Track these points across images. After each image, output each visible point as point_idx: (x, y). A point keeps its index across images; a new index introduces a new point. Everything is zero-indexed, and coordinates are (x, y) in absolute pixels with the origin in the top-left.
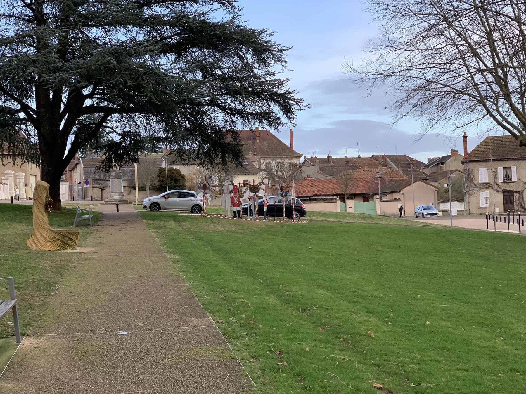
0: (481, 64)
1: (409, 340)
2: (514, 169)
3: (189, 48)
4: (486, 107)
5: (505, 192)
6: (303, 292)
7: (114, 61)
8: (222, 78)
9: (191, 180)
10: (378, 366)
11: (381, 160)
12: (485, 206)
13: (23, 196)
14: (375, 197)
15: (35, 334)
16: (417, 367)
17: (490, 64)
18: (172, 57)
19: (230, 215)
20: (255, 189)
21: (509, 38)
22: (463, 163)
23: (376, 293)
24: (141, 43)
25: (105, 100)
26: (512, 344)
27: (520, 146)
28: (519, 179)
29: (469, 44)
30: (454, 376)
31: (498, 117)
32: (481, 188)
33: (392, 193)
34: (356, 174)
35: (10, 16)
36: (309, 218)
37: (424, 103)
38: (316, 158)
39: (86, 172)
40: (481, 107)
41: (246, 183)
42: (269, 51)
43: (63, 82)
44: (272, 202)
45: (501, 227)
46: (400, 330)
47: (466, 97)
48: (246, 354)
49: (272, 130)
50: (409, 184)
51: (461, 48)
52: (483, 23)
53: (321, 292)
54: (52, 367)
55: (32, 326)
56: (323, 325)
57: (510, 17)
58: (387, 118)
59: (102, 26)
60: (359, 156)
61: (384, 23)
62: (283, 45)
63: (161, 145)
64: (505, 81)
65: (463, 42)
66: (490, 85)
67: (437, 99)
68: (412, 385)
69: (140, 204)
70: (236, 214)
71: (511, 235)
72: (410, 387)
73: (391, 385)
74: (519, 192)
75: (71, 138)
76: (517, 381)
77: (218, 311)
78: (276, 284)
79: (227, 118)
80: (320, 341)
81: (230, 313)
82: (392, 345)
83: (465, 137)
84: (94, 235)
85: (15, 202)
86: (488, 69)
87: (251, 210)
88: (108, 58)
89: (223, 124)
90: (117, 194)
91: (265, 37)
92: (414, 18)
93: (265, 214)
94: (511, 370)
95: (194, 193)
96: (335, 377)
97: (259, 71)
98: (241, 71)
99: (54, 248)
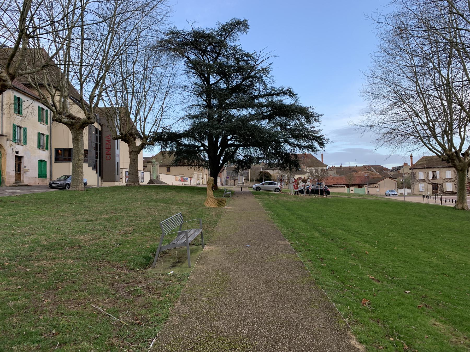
0: (420, 120)
1: (386, 256)
2: (438, 172)
3: (275, 117)
4: (423, 142)
5: (432, 184)
6: (331, 231)
7: (241, 124)
8: (290, 130)
9: (274, 177)
10: (371, 268)
11: (368, 168)
12: (422, 191)
13: (201, 183)
14: (364, 186)
15: (210, 244)
16: (391, 270)
17: (425, 120)
18: (267, 121)
19: (293, 193)
20: (305, 181)
21: (436, 108)
22: (410, 169)
23: (368, 233)
24: (253, 115)
25: (237, 141)
26: (441, 261)
27: (442, 161)
28: (441, 177)
29: (414, 112)
30: (411, 275)
31: (430, 147)
32: (420, 182)
33: (373, 184)
34: (355, 174)
35: (197, 105)
36: (332, 195)
37: (390, 140)
38: (334, 167)
39: (228, 173)
40: (421, 142)
41: (300, 179)
42: (313, 116)
43: (220, 134)
44: (313, 187)
45: (431, 202)
46: (382, 251)
47: (413, 137)
48: (306, 259)
49: (313, 154)
50: (383, 179)
51: (409, 113)
52: (422, 100)
53: (340, 231)
54: (218, 260)
55: (208, 241)
56: (342, 247)
57: (436, 97)
58: (371, 147)
59: (236, 108)
60: (356, 166)
61: (370, 102)
62: (319, 114)
63: (261, 161)
64: (434, 129)
65: (411, 110)
66: (425, 131)
67: (397, 138)
68: (389, 278)
69: (251, 187)
70: (296, 193)
71: (437, 206)
72: (389, 279)
73: (379, 278)
74: (440, 184)
75: (222, 158)
76: (446, 280)
77: (291, 238)
78: (318, 227)
79: (292, 148)
80: (341, 255)
81: (297, 239)
82: (378, 258)
83: (411, 156)
84: (232, 201)
85: (198, 186)
86: (424, 123)
87: (303, 191)
88: (239, 122)
89: (290, 151)
90: (241, 183)
91: (310, 110)
92: (385, 99)
93: (310, 193)
94: (442, 274)
95: (276, 183)
96: (350, 272)
97: (307, 126)
98: (299, 126)
99: (215, 206)
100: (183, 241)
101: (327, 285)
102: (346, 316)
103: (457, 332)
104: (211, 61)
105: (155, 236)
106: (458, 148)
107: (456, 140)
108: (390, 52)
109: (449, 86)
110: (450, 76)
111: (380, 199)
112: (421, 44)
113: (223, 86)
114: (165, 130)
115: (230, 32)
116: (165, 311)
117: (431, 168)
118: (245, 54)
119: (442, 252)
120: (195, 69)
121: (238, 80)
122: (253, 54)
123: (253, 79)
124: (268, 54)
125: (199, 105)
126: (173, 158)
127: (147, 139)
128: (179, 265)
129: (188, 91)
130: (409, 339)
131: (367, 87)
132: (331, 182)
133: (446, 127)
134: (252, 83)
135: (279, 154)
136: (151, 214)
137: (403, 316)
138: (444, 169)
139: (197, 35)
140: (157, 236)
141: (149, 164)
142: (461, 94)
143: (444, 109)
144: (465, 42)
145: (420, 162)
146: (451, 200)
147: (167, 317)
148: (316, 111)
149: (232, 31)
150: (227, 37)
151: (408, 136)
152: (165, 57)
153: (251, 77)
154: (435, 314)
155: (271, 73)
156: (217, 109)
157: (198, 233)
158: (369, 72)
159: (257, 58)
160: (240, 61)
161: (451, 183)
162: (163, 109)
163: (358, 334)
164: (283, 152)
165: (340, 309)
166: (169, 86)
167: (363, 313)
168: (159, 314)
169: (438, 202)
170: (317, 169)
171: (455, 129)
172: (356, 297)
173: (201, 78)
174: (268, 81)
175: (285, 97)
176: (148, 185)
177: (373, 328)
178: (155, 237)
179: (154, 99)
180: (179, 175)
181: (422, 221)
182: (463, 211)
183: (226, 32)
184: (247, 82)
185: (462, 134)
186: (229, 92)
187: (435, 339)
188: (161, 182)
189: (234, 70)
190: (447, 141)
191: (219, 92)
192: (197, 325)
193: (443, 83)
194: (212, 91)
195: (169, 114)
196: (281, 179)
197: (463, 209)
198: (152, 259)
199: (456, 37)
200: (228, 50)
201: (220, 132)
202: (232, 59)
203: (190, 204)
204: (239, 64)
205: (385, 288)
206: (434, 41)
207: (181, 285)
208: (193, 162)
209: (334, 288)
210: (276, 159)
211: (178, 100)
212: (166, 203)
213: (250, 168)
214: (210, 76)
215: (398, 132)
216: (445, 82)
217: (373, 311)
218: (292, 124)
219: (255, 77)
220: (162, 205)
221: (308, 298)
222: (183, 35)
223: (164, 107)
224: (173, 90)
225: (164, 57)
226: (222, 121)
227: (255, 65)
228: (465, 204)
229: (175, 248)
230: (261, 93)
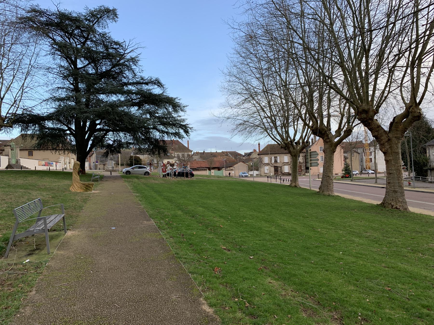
0: (266, 114)
2: (278, 157)
3: (144, 104)
4: (267, 132)
5: (275, 167)
7: (110, 109)
8: (159, 118)
10: (224, 240)
12: (267, 172)
14: (223, 169)
15: (74, 229)
16: (240, 239)
17: (269, 115)
18: (136, 108)
19: (162, 176)
20: (172, 165)
21: (277, 104)
22: (258, 155)
23: (223, 209)
28: (280, 161)
29: (261, 107)
30: (255, 243)
31: (272, 136)
33: (230, 167)
34: (215, 159)
35: (63, 88)
36: (196, 177)
40: (266, 132)
41: (168, 163)
42: (179, 106)
43: (88, 118)
44: (179, 171)
45: (273, 181)
46: (233, 224)
47: (260, 128)
48: (168, 236)
49: (180, 140)
51: (258, 108)
52: (267, 98)
53: (201, 209)
55: (72, 225)
56: (201, 223)
57: (277, 96)
58: (228, 136)
59: (105, 94)
60: (216, 152)
61: (227, 96)
62: (185, 105)
64: (275, 122)
65: (259, 106)
68: (238, 247)
69: (121, 171)
70: (164, 176)
71: (277, 184)
73: (230, 247)
74: (280, 167)
75: (90, 142)
79: (161, 135)
83: (259, 144)
85: (64, 170)
86: (268, 117)
87: (171, 174)
88: (107, 108)
91: (177, 101)
92: (239, 95)
95: (146, 167)
97: (174, 115)
98: (167, 115)
99: (82, 191)
100: (41, 228)
101: (185, 258)
102: (200, 284)
103: (287, 287)
104: (78, 45)
105: (9, 224)
106: (292, 138)
107: (291, 131)
108: (243, 55)
109: (287, 88)
110: (288, 79)
111: (234, 180)
112: (267, 51)
113: (91, 70)
114: (26, 112)
115: (99, 19)
116: (16, 303)
117: (273, 154)
118: (114, 42)
119: (279, 222)
120: (60, 51)
121: (107, 66)
122: (122, 43)
123: (122, 67)
124: (137, 45)
125: (65, 88)
126: (35, 141)
127: (4, 121)
128: (37, 252)
129: (52, 73)
130: (250, 297)
131: (224, 84)
132: (196, 166)
133: (284, 120)
134: (121, 71)
135: (148, 140)
136: (7, 200)
137: (246, 279)
138: (284, 155)
139: (63, 16)
140: (13, 224)
141: (7, 147)
142: (295, 94)
143: (283, 106)
144: (298, 53)
145: (266, 149)
146: (287, 180)
147: (18, 308)
148: (182, 101)
149: (101, 17)
150: (95, 23)
151: (256, 127)
152: (26, 35)
153: (120, 65)
154: (272, 274)
155: (140, 63)
156: (85, 93)
157: (59, 218)
158: (226, 71)
159: (126, 47)
160: (110, 48)
161: (288, 166)
162: (23, 89)
163: (209, 299)
164: (152, 138)
165: (195, 279)
166: (30, 66)
167: (215, 280)
168: (9, 307)
169: (278, 182)
170: (184, 154)
171: (290, 122)
172: (210, 266)
173: (68, 61)
174: (137, 70)
175: (154, 87)
176: (6, 169)
177: (222, 293)
178: (9, 225)
179: (13, 79)
180: (43, 160)
181: (266, 197)
182: (295, 188)
183: (94, 18)
184: (116, 69)
185: (296, 126)
186: (98, 77)
187: (270, 295)
188: (22, 167)
189: (103, 56)
190: (284, 133)
191: (87, 76)
192: (53, 313)
193: (282, 85)
194: (80, 75)
195: (30, 95)
196: (150, 164)
197: (296, 186)
198: (5, 248)
199: (292, 48)
200: (97, 36)
201: (87, 116)
202: (101, 46)
203: (54, 190)
204: (108, 51)
205: (234, 256)
206: (276, 49)
207: (37, 273)
208: (58, 146)
209: (191, 260)
210: (145, 144)
211: (42, 82)
212: (25, 189)
213: (119, 152)
214: (78, 60)
215: (249, 123)
216: (284, 84)
217: (223, 277)
218: (160, 112)
219: (125, 65)
220: (21, 190)
221: (168, 272)
222: (47, 14)
223: (24, 88)
224: (35, 70)
225: (25, 35)
226: (91, 105)
227: (124, 54)
228: (297, 183)
229: (33, 235)
230: (130, 81)
